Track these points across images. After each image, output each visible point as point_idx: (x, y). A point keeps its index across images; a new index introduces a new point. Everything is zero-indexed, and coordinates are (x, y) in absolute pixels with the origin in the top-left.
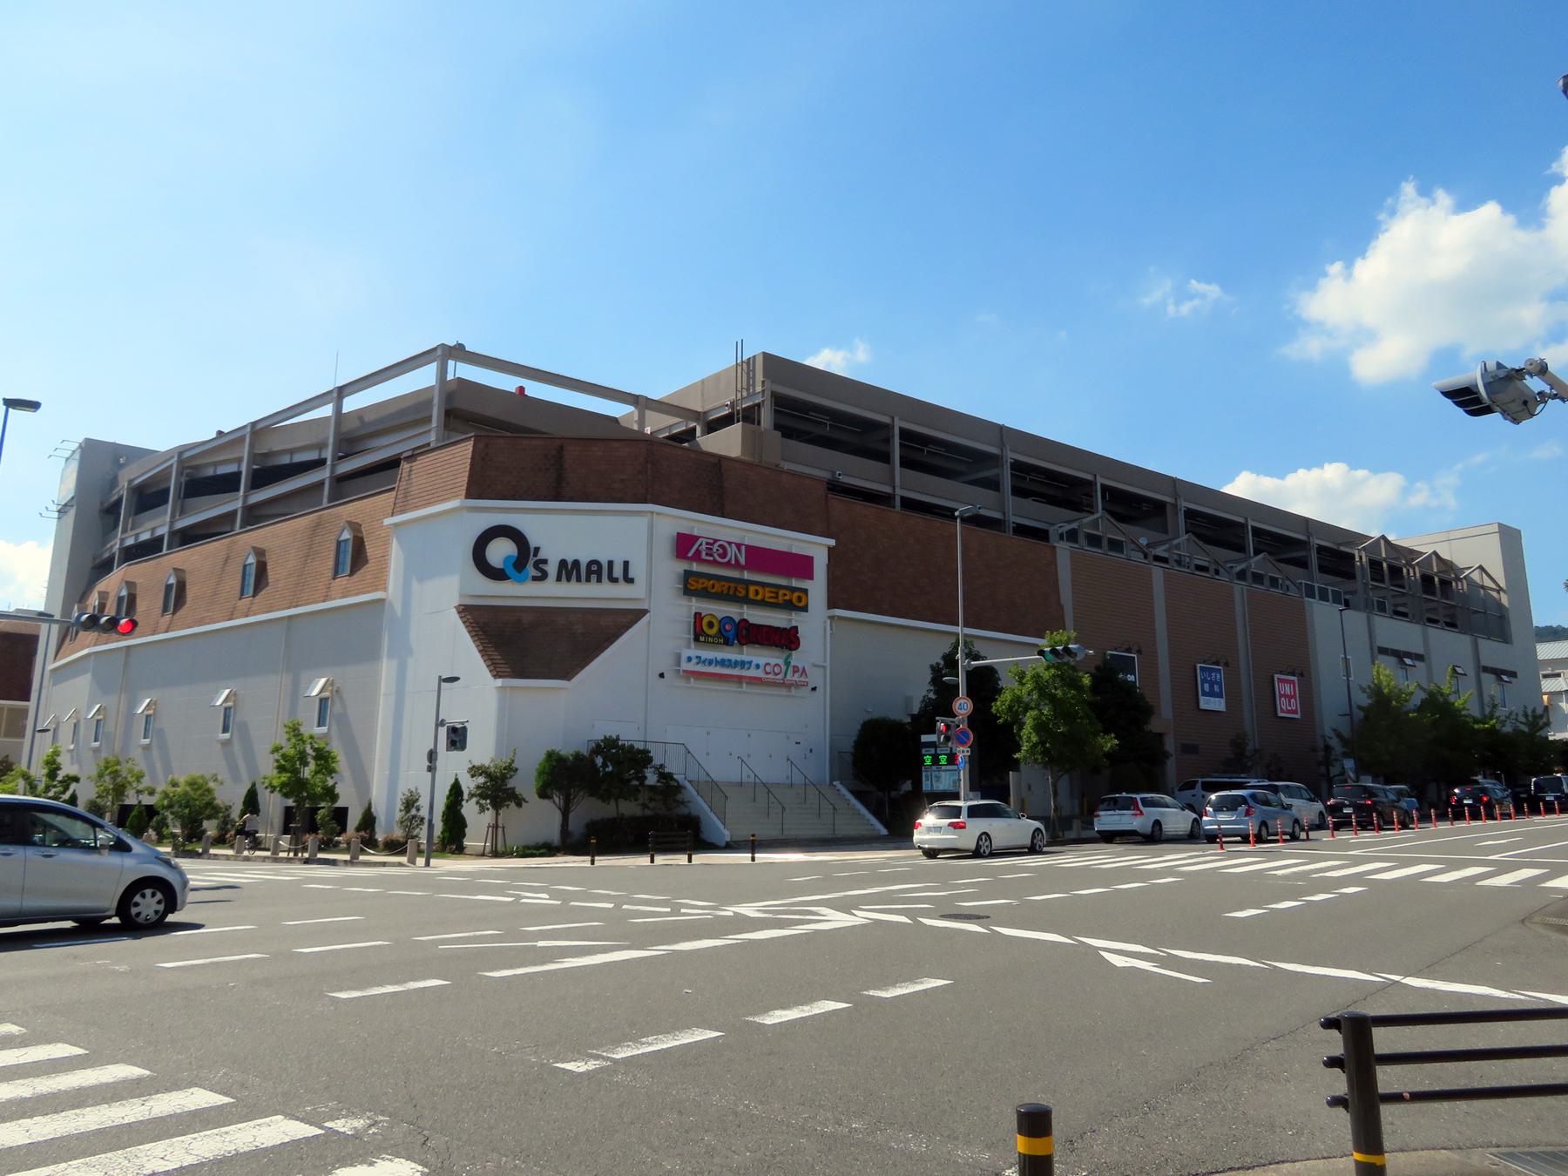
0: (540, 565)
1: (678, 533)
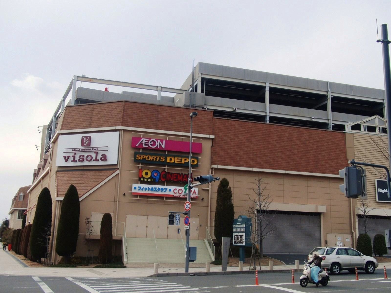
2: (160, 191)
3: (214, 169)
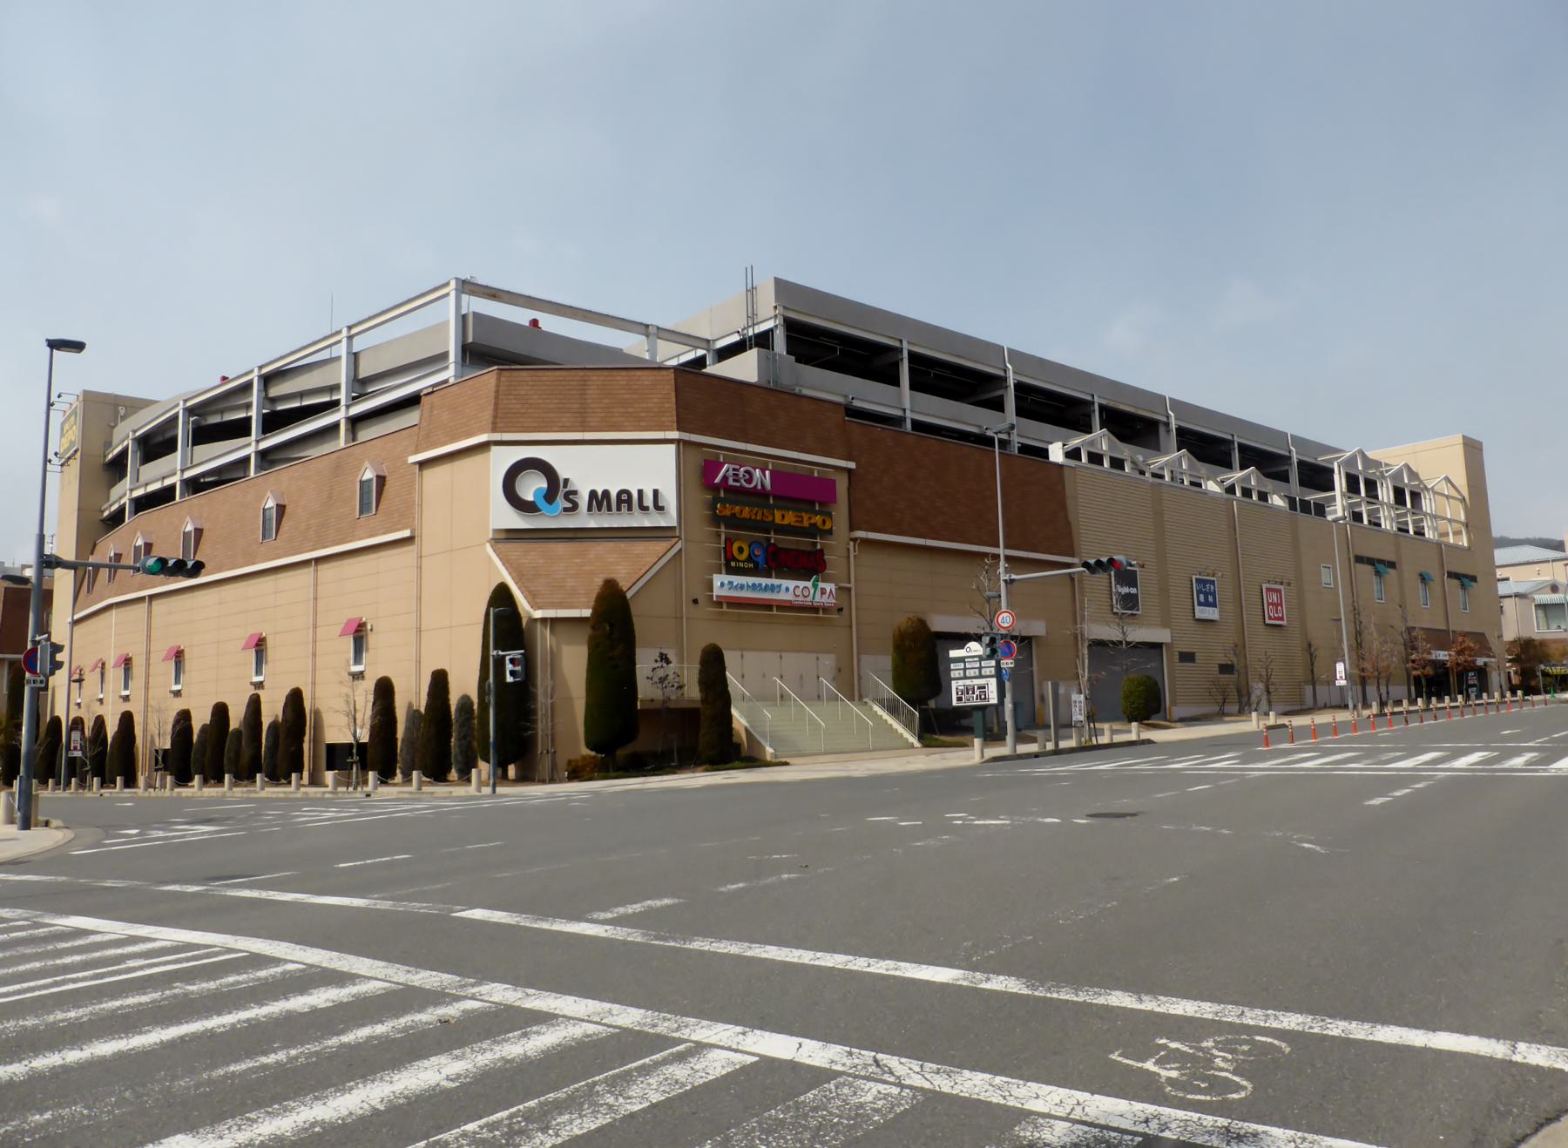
0: (571, 497)
3: (859, 541)
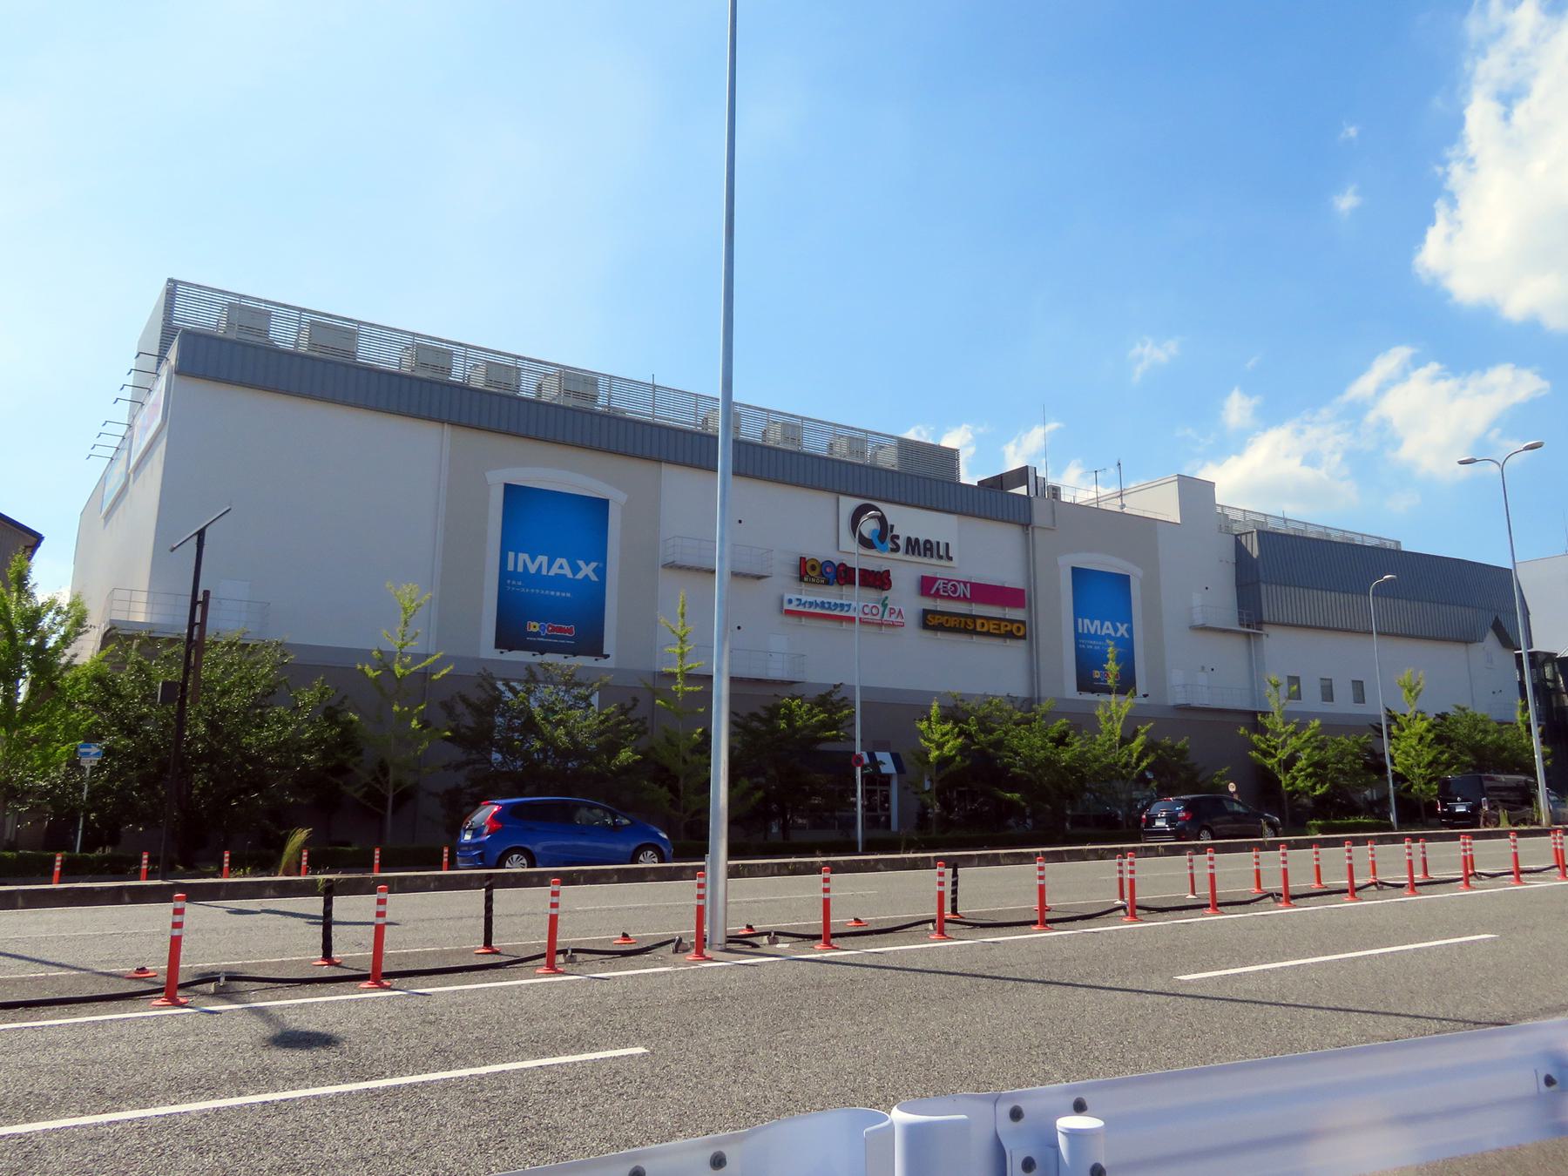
1: (922, 576)
2: (839, 609)
